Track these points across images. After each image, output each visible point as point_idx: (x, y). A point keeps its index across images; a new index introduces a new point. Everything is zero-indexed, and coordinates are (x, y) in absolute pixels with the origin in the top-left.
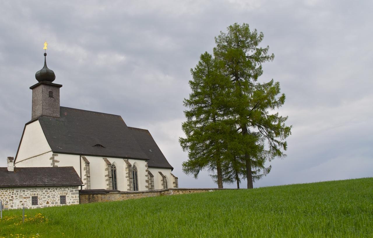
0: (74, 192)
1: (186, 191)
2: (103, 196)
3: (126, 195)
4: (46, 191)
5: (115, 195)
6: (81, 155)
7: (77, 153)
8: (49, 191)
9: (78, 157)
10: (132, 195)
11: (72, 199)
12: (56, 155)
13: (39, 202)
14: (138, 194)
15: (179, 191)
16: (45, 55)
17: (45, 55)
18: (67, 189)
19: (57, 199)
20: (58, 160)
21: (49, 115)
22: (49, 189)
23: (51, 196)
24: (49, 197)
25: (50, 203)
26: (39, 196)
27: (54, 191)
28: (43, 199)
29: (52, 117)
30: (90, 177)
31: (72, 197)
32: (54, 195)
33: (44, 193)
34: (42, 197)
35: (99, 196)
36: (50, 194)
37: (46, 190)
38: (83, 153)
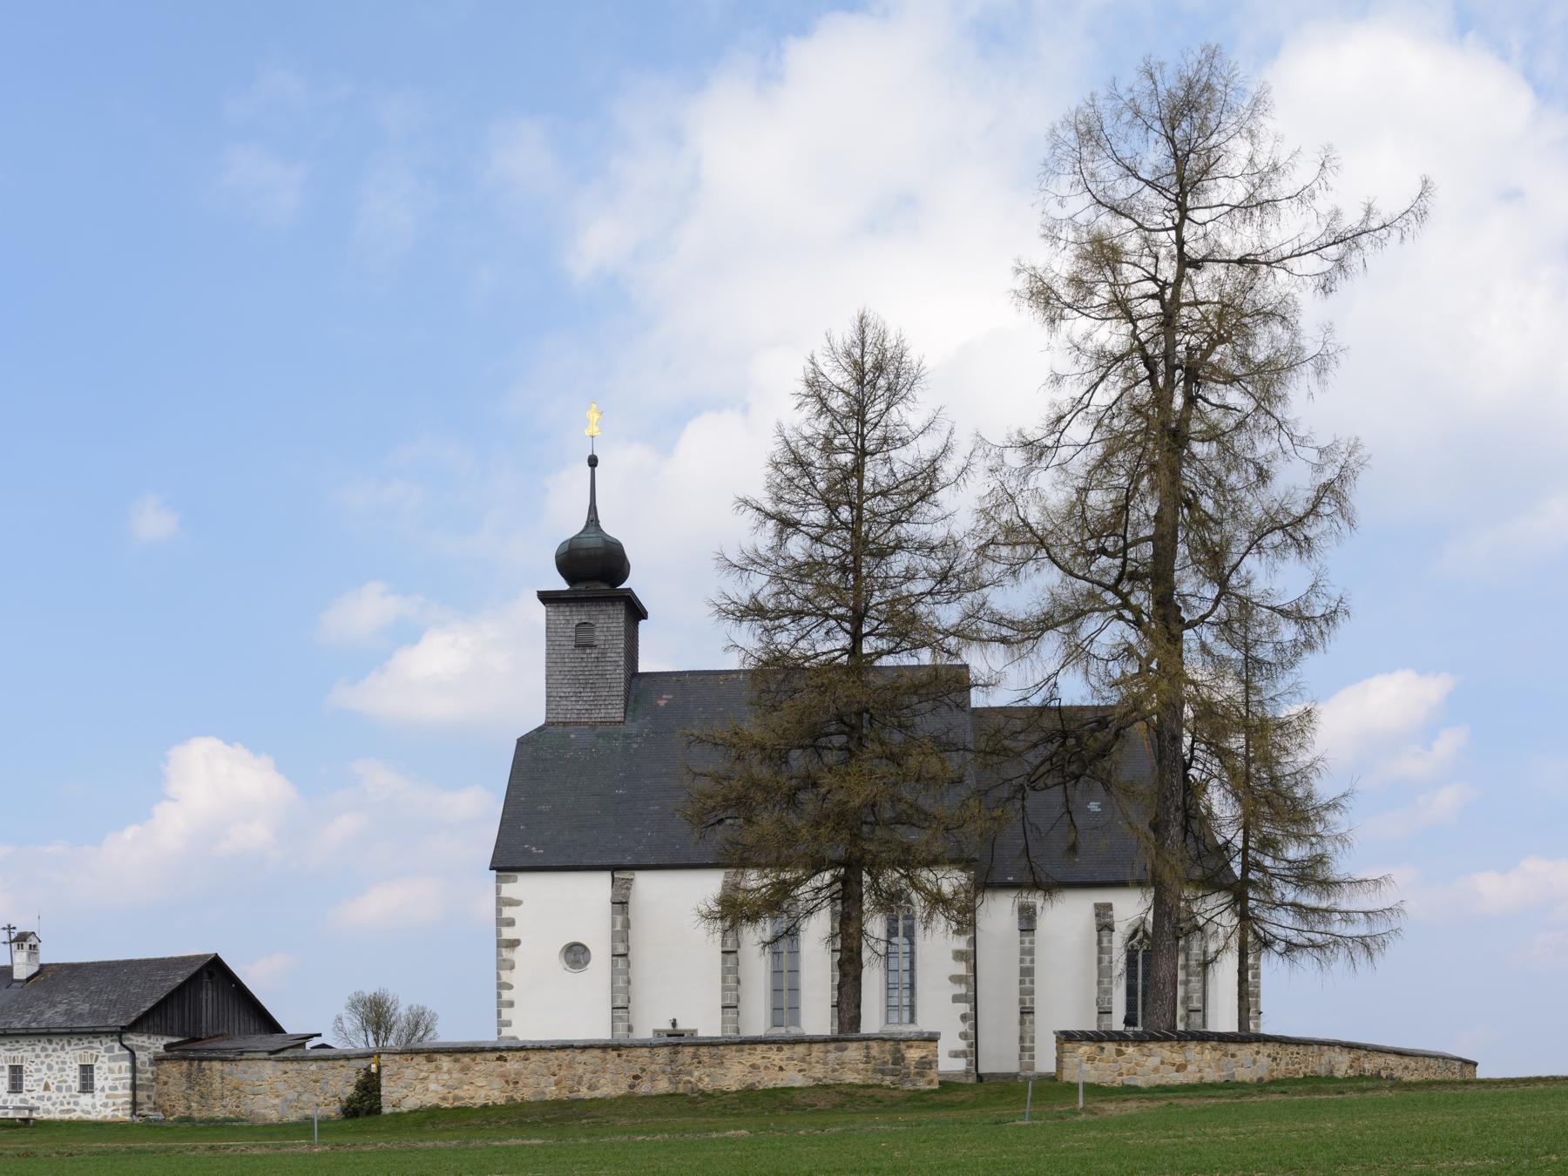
0: (117, 1052)
1: (479, 1057)
2: (227, 1067)
3: (296, 1066)
4: (44, 1049)
5: (260, 1064)
6: (613, 869)
7: (598, 862)
8: (50, 1048)
9: (604, 879)
10: (314, 1067)
11: (111, 1076)
12: (506, 881)
13: (27, 1083)
14: (330, 1063)
15: (437, 1056)
16: (593, 462)
17: (593, 462)
18: (96, 1044)
19: (72, 1074)
20: (515, 897)
21: (572, 717)
22: (50, 1042)
23: (56, 1067)
24: (50, 1068)
25: (53, 1088)
26: (25, 1065)
27: (63, 1048)
28: (37, 1076)
29: (585, 723)
30: (625, 955)
31: (111, 1071)
32: (64, 1063)
33: (38, 1056)
34: (33, 1067)
35: (217, 1065)
36: (52, 1060)
37: (41, 1045)
38: (618, 861)
